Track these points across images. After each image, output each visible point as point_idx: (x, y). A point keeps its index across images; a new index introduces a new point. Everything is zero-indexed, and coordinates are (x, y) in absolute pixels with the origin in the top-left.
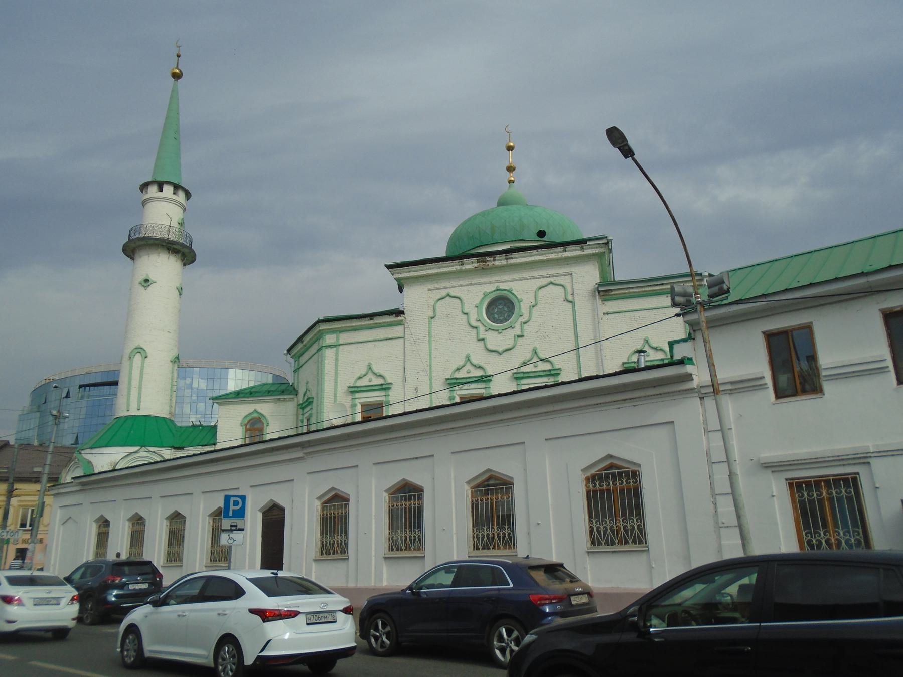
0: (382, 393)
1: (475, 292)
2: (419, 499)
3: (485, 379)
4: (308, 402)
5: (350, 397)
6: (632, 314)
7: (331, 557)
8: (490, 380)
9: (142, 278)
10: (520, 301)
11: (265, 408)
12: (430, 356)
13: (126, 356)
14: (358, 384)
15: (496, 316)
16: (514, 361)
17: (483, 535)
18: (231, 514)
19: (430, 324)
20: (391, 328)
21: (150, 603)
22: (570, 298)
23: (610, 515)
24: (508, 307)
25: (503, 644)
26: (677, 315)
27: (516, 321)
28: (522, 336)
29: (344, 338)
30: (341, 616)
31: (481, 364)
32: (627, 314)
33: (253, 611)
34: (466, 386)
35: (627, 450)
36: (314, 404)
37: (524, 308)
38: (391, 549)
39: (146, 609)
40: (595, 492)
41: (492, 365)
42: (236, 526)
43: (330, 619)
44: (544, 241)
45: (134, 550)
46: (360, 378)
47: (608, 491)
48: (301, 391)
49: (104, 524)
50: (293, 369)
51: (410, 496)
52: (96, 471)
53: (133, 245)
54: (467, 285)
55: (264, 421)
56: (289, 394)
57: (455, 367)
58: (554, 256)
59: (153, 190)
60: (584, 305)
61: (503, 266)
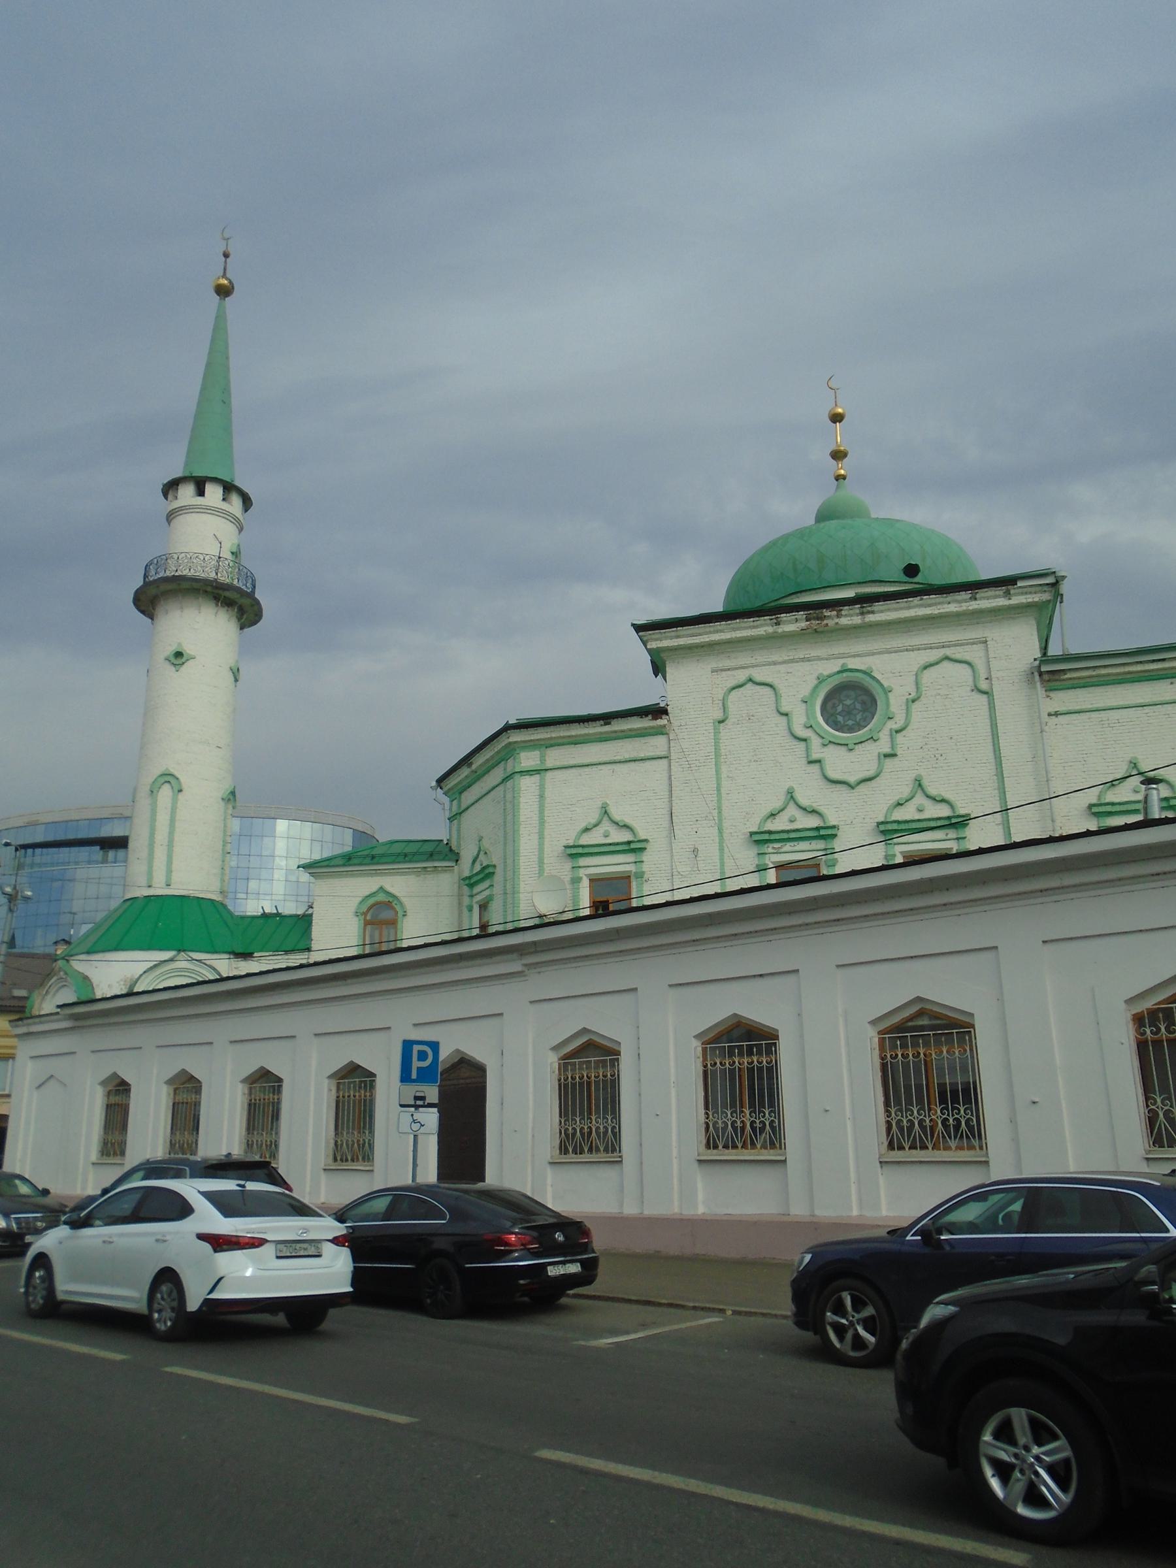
0: (630, 858)
1: (799, 673)
2: (769, 1052)
3: (958, 823)
4: (487, 873)
5: (568, 865)
6: (1103, 714)
7: (586, 1157)
8: (643, 849)
9: (170, 650)
10: (887, 691)
12: (719, 790)
13: (144, 791)
14: (583, 842)
15: (840, 718)
16: (876, 804)
17: (911, 1122)
18: (414, 1076)
19: (717, 732)
20: (643, 740)
21: (65, 1223)
22: (984, 686)
23: (920, 1101)
24: (863, 703)
25: (844, 1321)
28: (894, 755)
29: (555, 757)
30: (329, 1249)
31: (815, 806)
32: (1093, 715)
33: (202, 1237)
34: (788, 847)
36: (498, 878)
37: (896, 703)
38: (711, 1144)
39: (62, 1231)
41: (837, 808)
42: (423, 1098)
43: (312, 1251)
44: (915, 583)
45: (178, 1136)
46: (587, 830)
48: (467, 853)
49: (119, 1089)
50: (448, 815)
51: (750, 1048)
52: (99, 995)
53: (153, 591)
54: (784, 662)
55: (398, 908)
56: (443, 860)
57: (766, 811)
58: (952, 608)
59: (186, 493)
60: (1015, 701)
61: (855, 627)
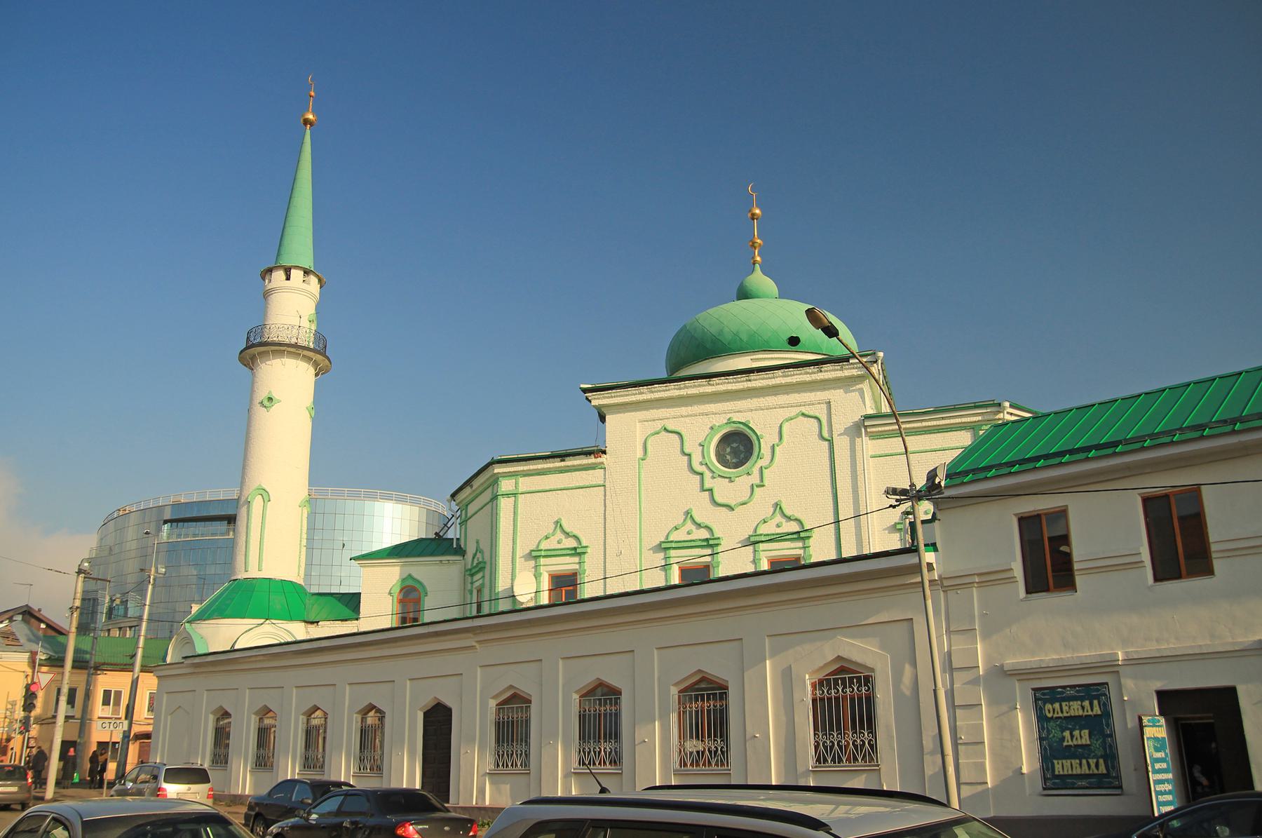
0: (576, 559)
2: (616, 703)
3: (351, 602)
8: (809, 537)
11: (428, 571)
23: (839, 729)
26: (912, 485)
27: (754, 466)
29: (525, 483)
35: (863, 650)
37: (765, 450)
40: (822, 700)
47: (837, 699)
51: (696, 697)
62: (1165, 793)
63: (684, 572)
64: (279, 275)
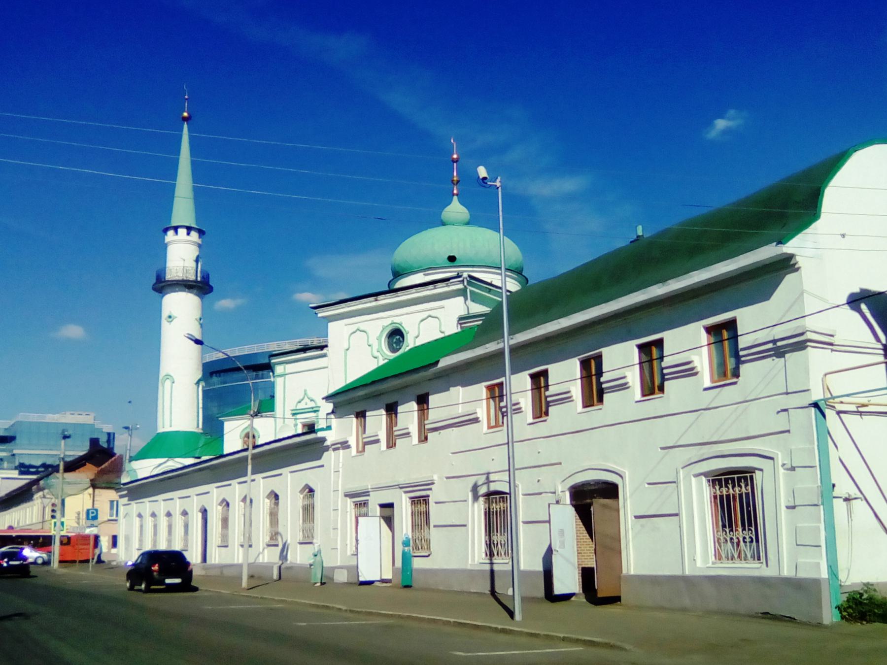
23: (730, 526)
29: (290, 368)
62: (263, 558)
63: (304, 425)
64: (171, 233)
